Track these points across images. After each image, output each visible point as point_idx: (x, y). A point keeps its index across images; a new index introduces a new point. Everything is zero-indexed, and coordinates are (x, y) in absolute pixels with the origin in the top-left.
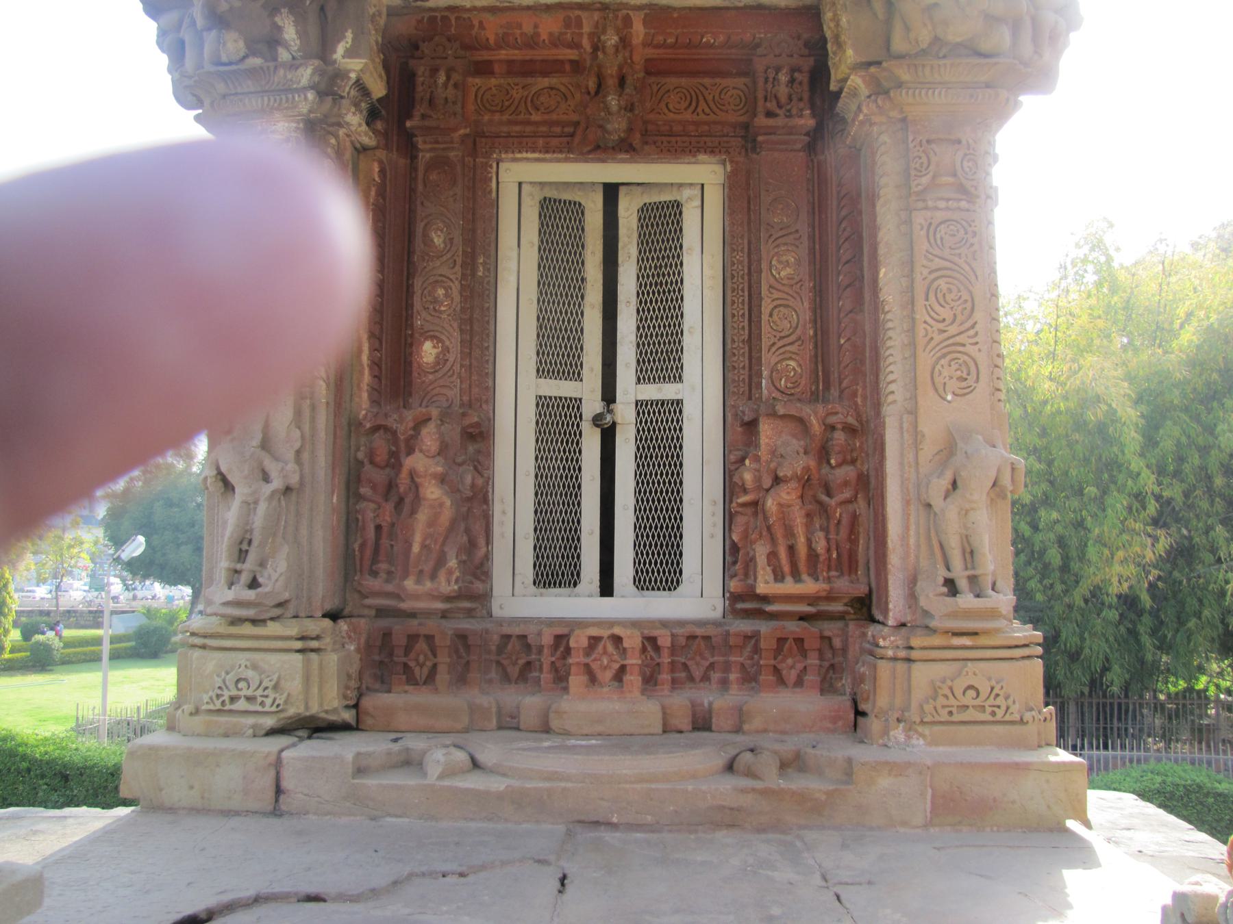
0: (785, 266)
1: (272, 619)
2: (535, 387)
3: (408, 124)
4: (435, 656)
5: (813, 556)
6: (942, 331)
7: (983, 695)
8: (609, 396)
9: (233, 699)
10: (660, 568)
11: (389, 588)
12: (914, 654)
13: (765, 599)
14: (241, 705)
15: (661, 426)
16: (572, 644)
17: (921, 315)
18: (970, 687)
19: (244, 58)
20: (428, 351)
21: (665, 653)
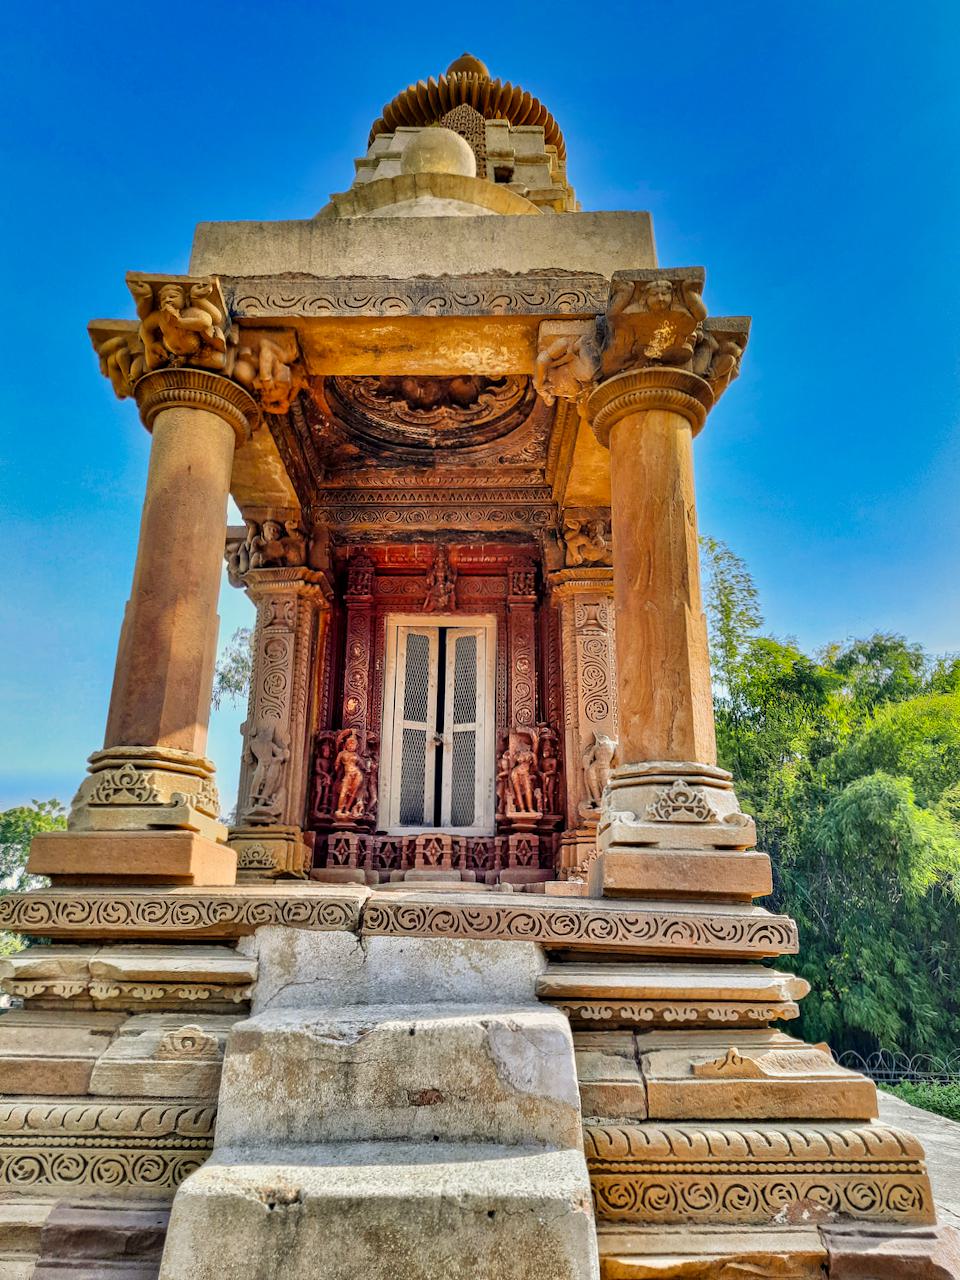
0: (523, 667)
5: (534, 800)
8: (440, 728)
9: (251, 862)
11: (328, 816)
14: (255, 865)
15: (466, 740)
17: (580, 683)
20: (351, 705)
21: (463, 850)
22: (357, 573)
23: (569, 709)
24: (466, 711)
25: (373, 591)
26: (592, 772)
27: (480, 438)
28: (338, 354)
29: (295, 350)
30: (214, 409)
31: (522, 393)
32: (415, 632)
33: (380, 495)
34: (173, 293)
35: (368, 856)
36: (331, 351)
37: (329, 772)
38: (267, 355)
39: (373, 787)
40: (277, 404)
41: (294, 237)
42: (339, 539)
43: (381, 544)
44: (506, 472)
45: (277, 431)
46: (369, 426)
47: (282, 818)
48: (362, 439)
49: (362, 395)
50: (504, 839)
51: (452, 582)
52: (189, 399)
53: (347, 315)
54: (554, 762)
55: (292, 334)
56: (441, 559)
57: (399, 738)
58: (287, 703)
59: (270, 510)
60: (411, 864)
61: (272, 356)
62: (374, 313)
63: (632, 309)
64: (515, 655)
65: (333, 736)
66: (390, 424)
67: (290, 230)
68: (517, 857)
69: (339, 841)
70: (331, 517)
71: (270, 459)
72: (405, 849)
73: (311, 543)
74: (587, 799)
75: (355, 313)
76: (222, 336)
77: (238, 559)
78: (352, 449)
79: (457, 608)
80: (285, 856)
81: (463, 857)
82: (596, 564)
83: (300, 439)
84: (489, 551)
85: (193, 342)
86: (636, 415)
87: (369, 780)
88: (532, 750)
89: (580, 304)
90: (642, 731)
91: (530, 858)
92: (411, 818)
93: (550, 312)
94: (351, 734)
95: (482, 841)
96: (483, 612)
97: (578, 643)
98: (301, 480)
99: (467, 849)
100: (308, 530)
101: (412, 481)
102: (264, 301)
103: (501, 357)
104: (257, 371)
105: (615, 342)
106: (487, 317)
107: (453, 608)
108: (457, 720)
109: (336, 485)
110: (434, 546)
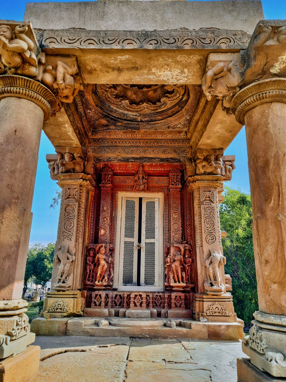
0: (176, 216)
1: (67, 290)
2: (124, 239)
3: (100, 185)
4: (101, 299)
5: (182, 277)
6: (207, 230)
7: (220, 310)
8: (140, 241)
10: (150, 281)
11: (92, 283)
12: (204, 300)
13: (173, 287)
14: (59, 310)
15: (151, 248)
16: (131, 296)
17: (203, 226)
18: (217, 307)
19: (74, 87)
20: (102, 232)
21: (151, 299)
22: (106, 175)
23: (198, 238)
24: (151, 233)
25: (112, 182)
26: (211, 269)
27: (160, 118)
28: (99, 72)
29: (76, 68)
30: (31, 98)
31: (181, 97)
32: (129, 199)
33: (116, 142)
34: (5, 29)
35: (110, 302)
36: (95, 70)
37: (92, 263)
38: (61, 70)
39: (111, 270)
40: (67, 97)
41: (77, 11)
42: (98, 160)
43: (115, 162)
44: (170, 132)
45: (69, 112)
46: (111, 111)
47: (71, 287)
48: (109, 117)
49: (109, 97)
50: (169, 294)
51: (146, 179)
52: (16, 93)
53: (104, 48)
54: (190, 260)
55: (74, 59)
56: (141, 169)
57: (123, 245)
58: (74, 234)
59: (67, 148)
60: (128, 306)
61: (64, 70)
62: (119, 47)
63: (270, 43)
64: (172, 211)
65: (94, 246)
66: (121, 111)
67: (75, 6)
68: (175, 304)
69: (96, 295)
70: (94, 151)
71: (67, 125)
72: (125, 298)
73: (86, 162)
74: (208, 281)
75: (108, 47)
76: (34, 56)
77: (54, 168)
78: (104, 121)
79: (147, 190)
80: (72, 306)
81: (151, 302)
82: (209, 174)
83: (81, 118)
84: (161, 166)
85: (18, 60)
86: (265, 105)
87: (110, 266)
88: (181, 254)
89: (232, 43)
90: (280, 295)
91: (181, 304)
92: (127, 281)
93: (215, 48)
94: (102, 246)
95: (159, 294)
96: (158, 191)
97: (202, 208)
98: (81, 135)
99: (153, 299)
100: (85, 157)
101: (129, 136)
102: (59, 40)
103: (183, 75)
104: (55, 79)
105: (255, 63)
106: (180, 50)
107: (146, 190)
108: (147, 238)
109: (96, 137)
110: (138, 163)
